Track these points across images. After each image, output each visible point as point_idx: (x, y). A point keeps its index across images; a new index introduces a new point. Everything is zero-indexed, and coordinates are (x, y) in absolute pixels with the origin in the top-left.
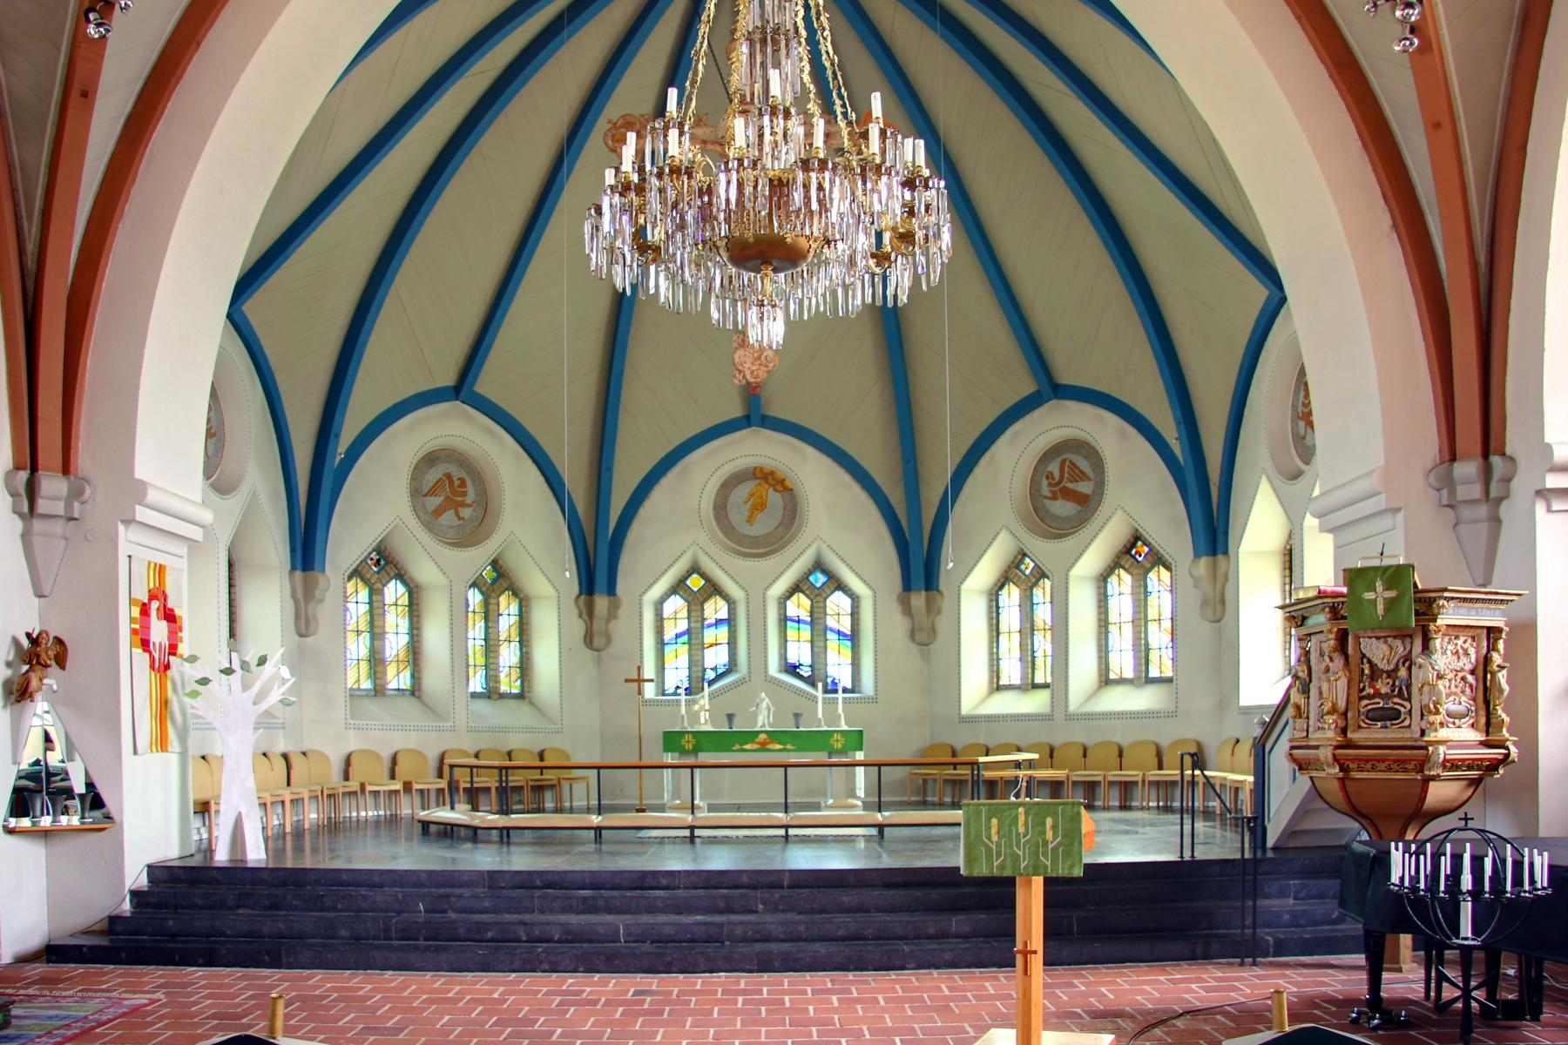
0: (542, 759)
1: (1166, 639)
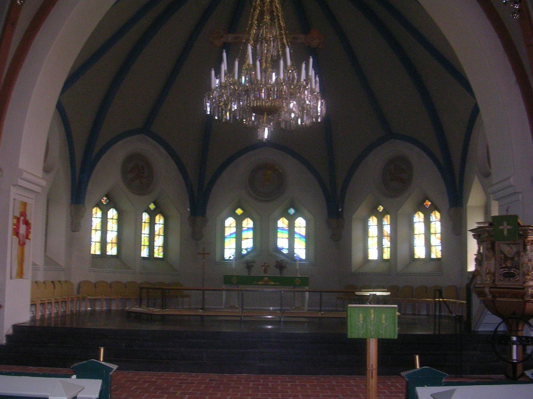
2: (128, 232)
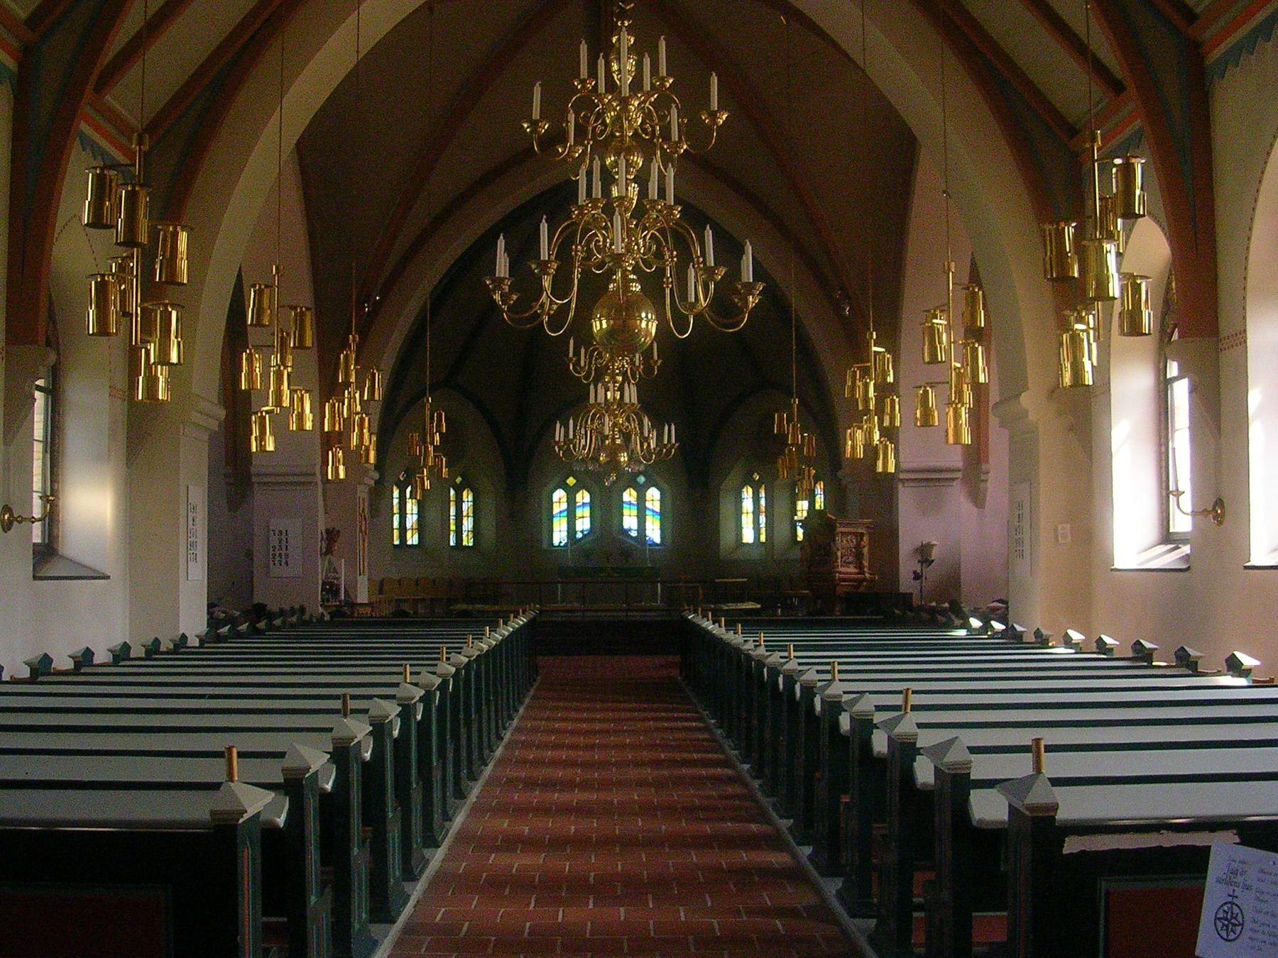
2: (433, 514)
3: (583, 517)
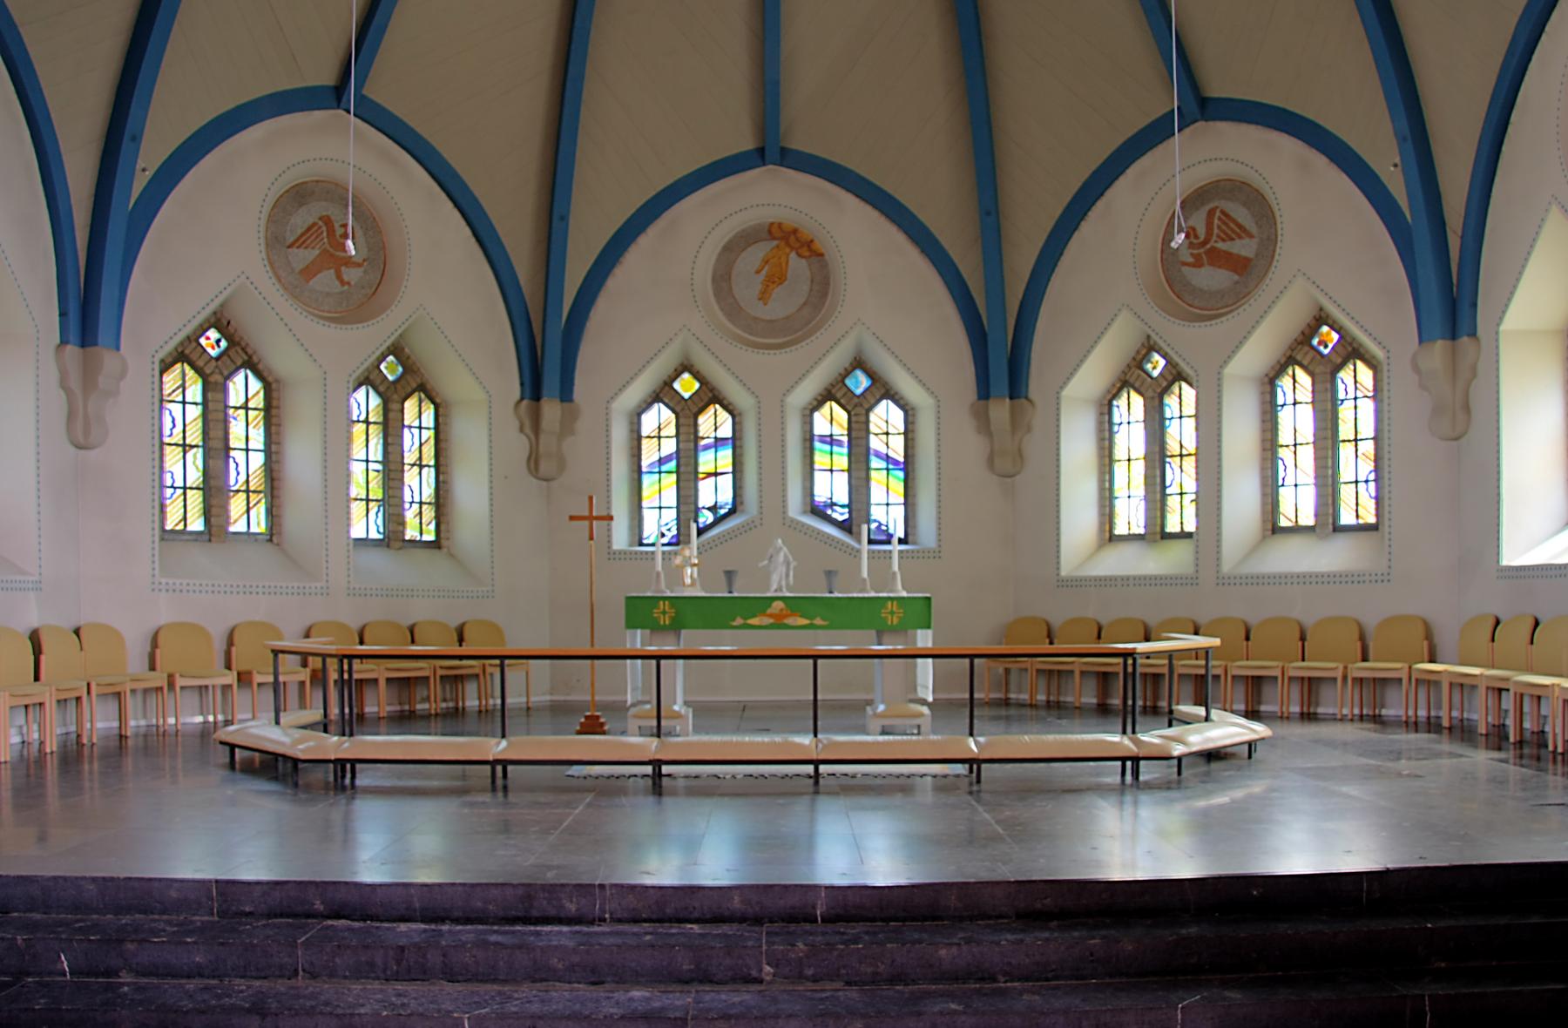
0: (461, 640)
1: (1366, 468)
3: (716, 474)
